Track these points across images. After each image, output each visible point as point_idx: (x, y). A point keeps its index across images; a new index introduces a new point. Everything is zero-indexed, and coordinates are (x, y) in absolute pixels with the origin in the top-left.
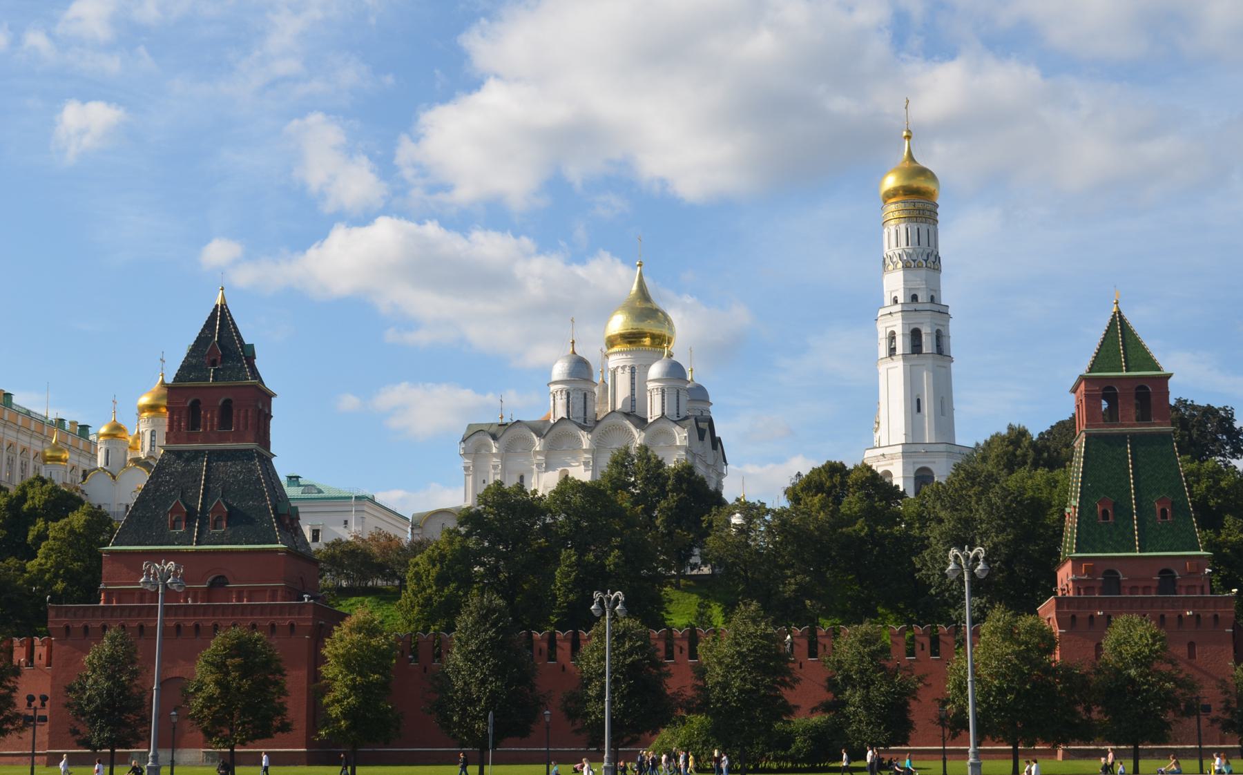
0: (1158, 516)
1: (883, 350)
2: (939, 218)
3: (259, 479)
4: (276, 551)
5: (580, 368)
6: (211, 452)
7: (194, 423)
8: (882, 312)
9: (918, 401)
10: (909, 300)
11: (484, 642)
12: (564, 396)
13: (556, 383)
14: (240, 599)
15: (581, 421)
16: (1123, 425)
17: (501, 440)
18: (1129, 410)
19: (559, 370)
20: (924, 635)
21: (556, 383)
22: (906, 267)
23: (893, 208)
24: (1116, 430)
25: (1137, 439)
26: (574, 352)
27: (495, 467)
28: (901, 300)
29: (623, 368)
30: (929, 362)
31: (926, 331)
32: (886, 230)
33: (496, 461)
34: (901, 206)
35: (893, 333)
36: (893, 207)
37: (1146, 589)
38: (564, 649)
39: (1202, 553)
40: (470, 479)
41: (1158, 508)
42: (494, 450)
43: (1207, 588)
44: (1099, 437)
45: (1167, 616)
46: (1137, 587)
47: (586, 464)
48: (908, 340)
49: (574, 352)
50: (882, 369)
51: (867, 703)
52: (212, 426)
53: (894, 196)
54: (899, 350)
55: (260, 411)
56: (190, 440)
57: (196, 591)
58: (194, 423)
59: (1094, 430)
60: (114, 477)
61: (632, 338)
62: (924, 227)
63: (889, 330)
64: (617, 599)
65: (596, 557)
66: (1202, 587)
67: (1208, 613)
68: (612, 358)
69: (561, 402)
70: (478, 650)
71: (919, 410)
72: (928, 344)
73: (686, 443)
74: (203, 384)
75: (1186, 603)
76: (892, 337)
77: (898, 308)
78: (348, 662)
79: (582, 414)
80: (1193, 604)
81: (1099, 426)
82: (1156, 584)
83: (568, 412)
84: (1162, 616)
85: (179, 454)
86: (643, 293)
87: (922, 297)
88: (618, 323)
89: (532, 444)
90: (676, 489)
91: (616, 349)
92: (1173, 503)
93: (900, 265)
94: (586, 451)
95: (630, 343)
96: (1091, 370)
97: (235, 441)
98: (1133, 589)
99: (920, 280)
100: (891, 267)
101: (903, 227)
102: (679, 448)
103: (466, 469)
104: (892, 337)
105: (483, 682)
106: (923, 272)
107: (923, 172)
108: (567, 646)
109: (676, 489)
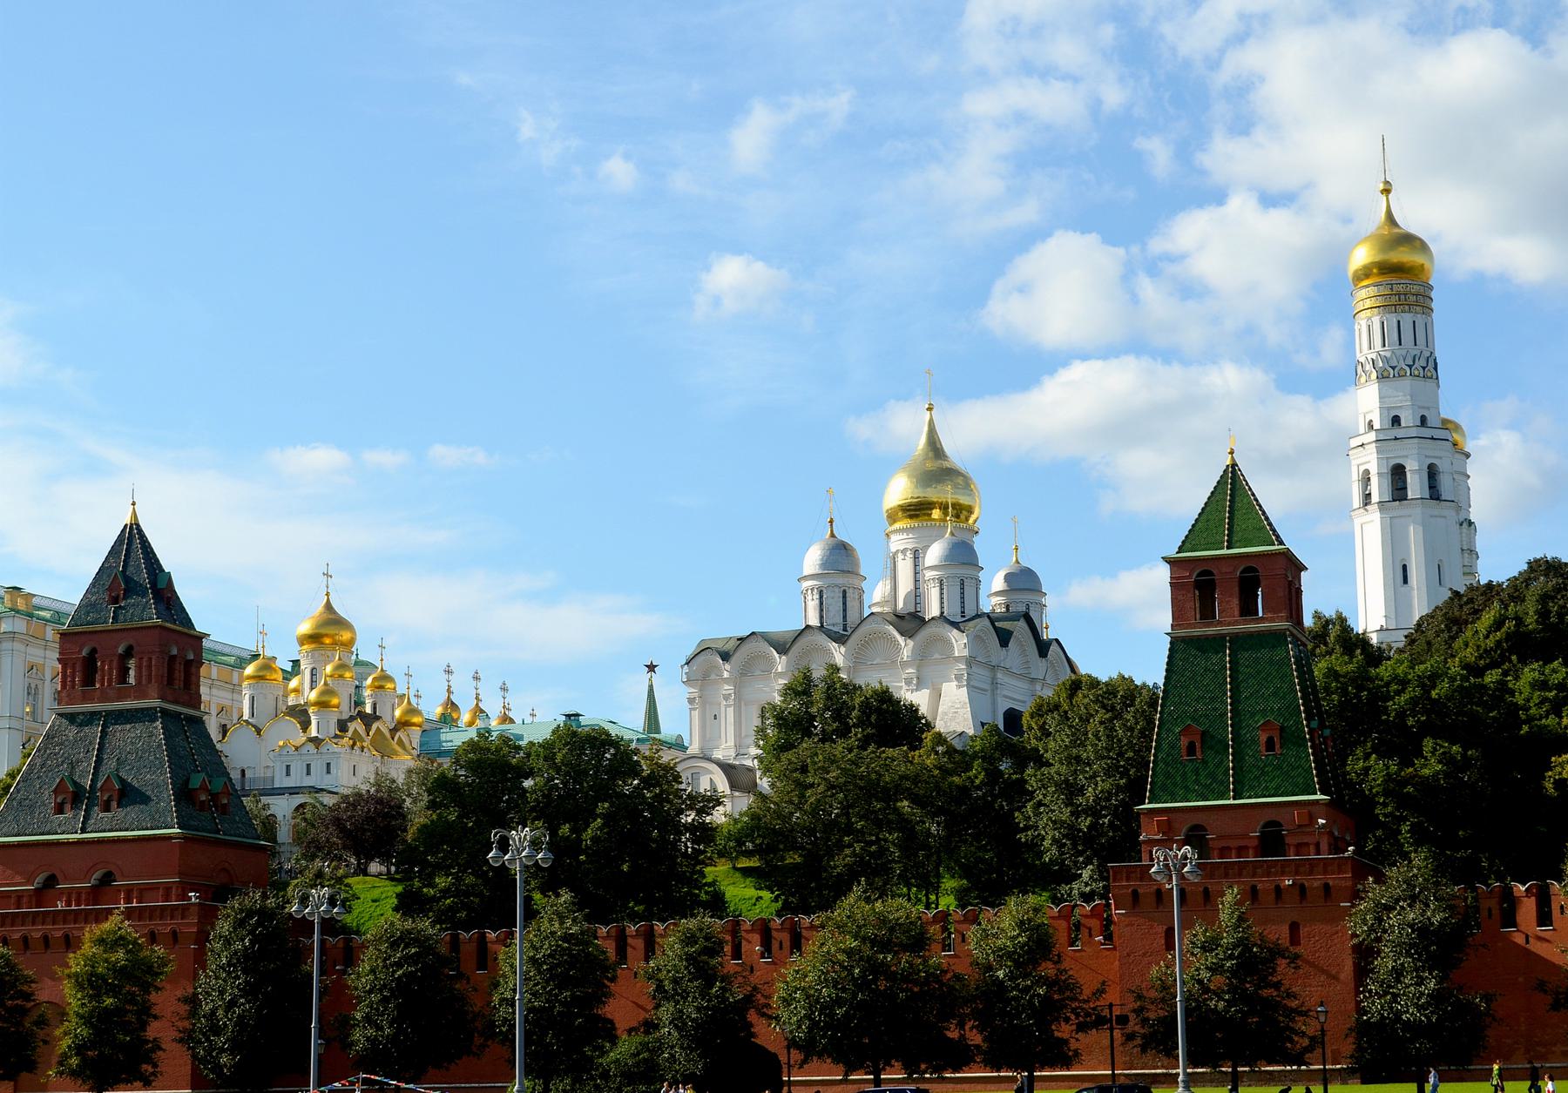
0: (1184, 752)
1: (1357, 501)
2: (1433, 305)
3: (160, 745)
4: (168, 838)
5: (841, 556)
6: (109, 713)
7: (88, 680)
8: (1355, 442)
9: (1405, 567)
10: (1388, 424)
11: (236, 953)
12: (816, 596)
13: (806, 578)
14: (128, 900)
15: (838, 629)
16: (1220, 623)
17: (733, 659)
18: (1226, 602)
19: (812, 559)
20: (782, 930)
21: (806, 578)
22: (1382, 377)
23: (1366, 295)
24: (1211, 630)
25: (1240, 642)
26: (833, 535)
27: (726, 697)
28: (1377, 426)
29: (904, 551)
30: (1417, 511)
31: (1411, 466)
32: (1357, 327)
33: (728, 688)
34: (1373, 291)
35: (1367, 472)
36: (1363, 293)
37: (1241, 851)
38: (1527, 910)
39: (1319, 796)
40: (696, 714)
41: (1263, 738)
42: (726, 675)
43: (1324, 846)
44: (1184, 640)
45: (1259, 886)
46: (1229, 849)
47: (958, 678)
48: (1387, 482)
49: (833, 535)
50: (1357, 522)
51: (678, 1021)
52: (110, 681)
53: (1367, 276)
54: (1375, 498)
55: (173, 658)
56: (86, 698)
57: (79, 891)
58: (88, 680)
59: (1182, 632)
60: (258, 731)
61: (916, 510)
62: (1407, 319)
63: (1362, 468)
64: (1185, 857)
65: (572, 830)
66: (1317, 845)
67: (1315, 882)
68: (894, 537)
69: (813, 604)
70: (229, 964)
71: (1405, 581)
72: (1415, 485)
73: (966, 653)
74: (99, 627)
75: (1284, 869)
76: (1366, 479)
77: (1372, 436)
78: (93, 983)
79: (840, 619)
80: (1296, 868)
81: (1190, 626)
82: (1256, 842)
83: (821, 617)
84: (1254, 888)
85: (71, 718)
86: (935, 447)
87: (1407, 419)
88: (899, 490)
89: (772, 663)
90: (861, 723)
91: (897, 526)
92: (1282, 729)
93: (1374, 376)
94: (726, 681)
95: (911, 517)
96: (1180, 550)
97: (136, 698)
98: (1224, 852)
99: (1403, 398)
100: (1363, 379)
101: (1376, 321)
102: (957, 659)
103: (691, 701)
104: (1366, 479)
105: (232, 1004)
106: (1407, 383)
107: (1408, 240)
108: (639, 943)
109: (861, 723)
